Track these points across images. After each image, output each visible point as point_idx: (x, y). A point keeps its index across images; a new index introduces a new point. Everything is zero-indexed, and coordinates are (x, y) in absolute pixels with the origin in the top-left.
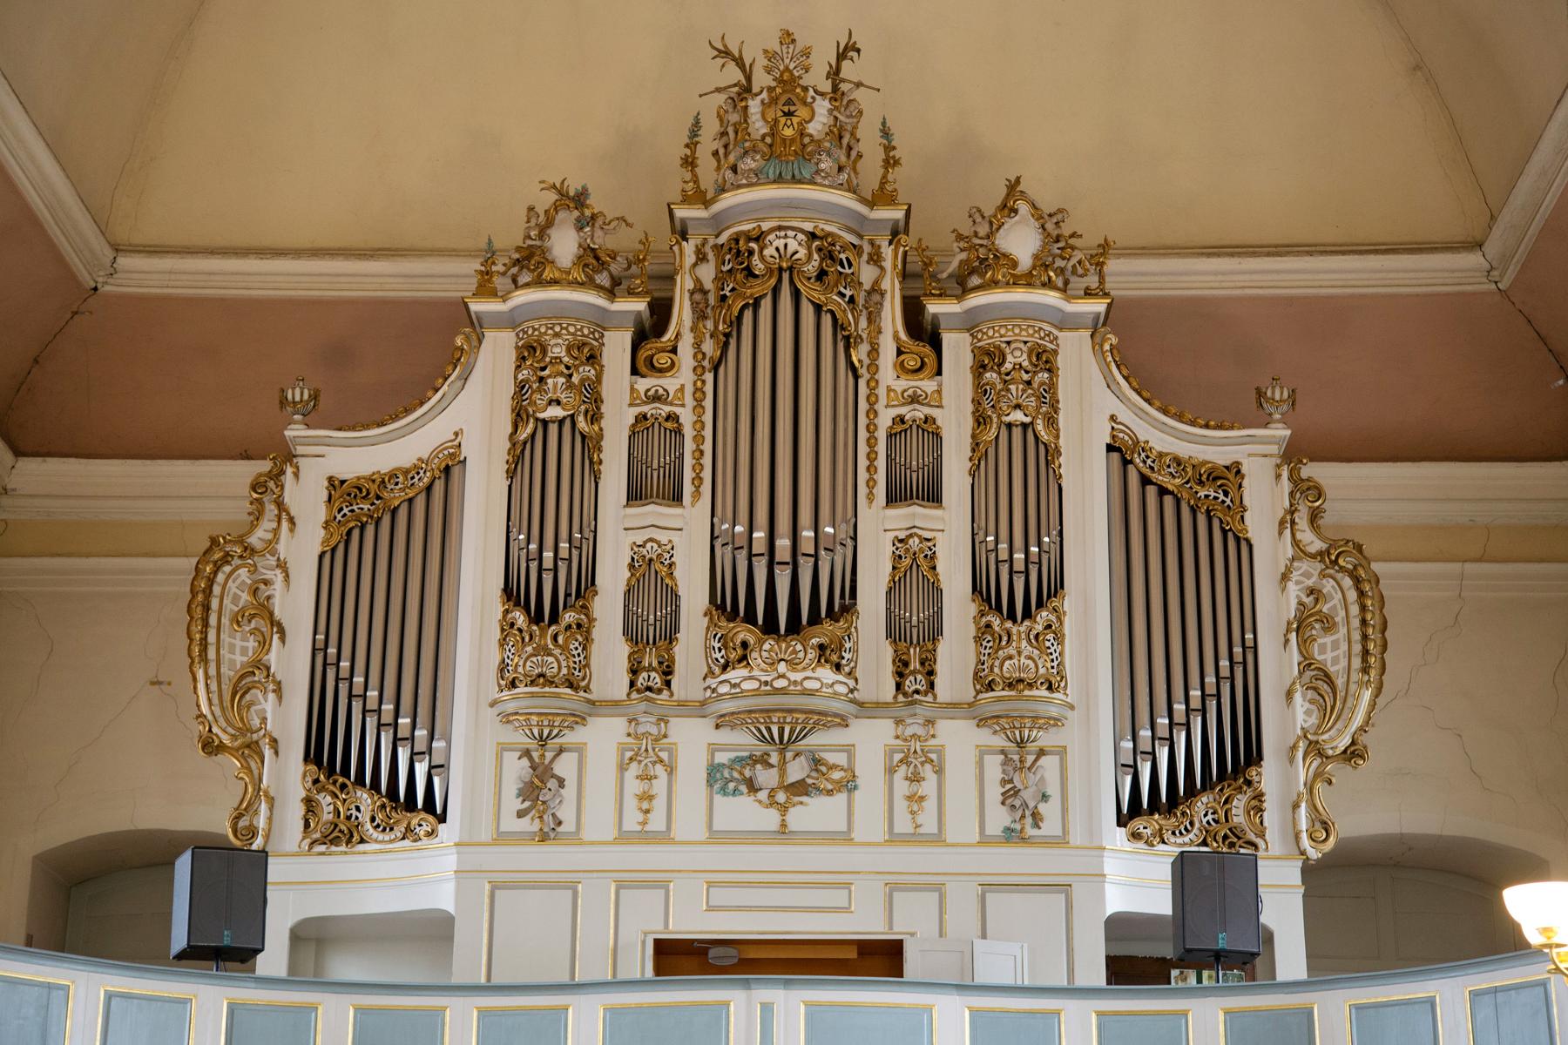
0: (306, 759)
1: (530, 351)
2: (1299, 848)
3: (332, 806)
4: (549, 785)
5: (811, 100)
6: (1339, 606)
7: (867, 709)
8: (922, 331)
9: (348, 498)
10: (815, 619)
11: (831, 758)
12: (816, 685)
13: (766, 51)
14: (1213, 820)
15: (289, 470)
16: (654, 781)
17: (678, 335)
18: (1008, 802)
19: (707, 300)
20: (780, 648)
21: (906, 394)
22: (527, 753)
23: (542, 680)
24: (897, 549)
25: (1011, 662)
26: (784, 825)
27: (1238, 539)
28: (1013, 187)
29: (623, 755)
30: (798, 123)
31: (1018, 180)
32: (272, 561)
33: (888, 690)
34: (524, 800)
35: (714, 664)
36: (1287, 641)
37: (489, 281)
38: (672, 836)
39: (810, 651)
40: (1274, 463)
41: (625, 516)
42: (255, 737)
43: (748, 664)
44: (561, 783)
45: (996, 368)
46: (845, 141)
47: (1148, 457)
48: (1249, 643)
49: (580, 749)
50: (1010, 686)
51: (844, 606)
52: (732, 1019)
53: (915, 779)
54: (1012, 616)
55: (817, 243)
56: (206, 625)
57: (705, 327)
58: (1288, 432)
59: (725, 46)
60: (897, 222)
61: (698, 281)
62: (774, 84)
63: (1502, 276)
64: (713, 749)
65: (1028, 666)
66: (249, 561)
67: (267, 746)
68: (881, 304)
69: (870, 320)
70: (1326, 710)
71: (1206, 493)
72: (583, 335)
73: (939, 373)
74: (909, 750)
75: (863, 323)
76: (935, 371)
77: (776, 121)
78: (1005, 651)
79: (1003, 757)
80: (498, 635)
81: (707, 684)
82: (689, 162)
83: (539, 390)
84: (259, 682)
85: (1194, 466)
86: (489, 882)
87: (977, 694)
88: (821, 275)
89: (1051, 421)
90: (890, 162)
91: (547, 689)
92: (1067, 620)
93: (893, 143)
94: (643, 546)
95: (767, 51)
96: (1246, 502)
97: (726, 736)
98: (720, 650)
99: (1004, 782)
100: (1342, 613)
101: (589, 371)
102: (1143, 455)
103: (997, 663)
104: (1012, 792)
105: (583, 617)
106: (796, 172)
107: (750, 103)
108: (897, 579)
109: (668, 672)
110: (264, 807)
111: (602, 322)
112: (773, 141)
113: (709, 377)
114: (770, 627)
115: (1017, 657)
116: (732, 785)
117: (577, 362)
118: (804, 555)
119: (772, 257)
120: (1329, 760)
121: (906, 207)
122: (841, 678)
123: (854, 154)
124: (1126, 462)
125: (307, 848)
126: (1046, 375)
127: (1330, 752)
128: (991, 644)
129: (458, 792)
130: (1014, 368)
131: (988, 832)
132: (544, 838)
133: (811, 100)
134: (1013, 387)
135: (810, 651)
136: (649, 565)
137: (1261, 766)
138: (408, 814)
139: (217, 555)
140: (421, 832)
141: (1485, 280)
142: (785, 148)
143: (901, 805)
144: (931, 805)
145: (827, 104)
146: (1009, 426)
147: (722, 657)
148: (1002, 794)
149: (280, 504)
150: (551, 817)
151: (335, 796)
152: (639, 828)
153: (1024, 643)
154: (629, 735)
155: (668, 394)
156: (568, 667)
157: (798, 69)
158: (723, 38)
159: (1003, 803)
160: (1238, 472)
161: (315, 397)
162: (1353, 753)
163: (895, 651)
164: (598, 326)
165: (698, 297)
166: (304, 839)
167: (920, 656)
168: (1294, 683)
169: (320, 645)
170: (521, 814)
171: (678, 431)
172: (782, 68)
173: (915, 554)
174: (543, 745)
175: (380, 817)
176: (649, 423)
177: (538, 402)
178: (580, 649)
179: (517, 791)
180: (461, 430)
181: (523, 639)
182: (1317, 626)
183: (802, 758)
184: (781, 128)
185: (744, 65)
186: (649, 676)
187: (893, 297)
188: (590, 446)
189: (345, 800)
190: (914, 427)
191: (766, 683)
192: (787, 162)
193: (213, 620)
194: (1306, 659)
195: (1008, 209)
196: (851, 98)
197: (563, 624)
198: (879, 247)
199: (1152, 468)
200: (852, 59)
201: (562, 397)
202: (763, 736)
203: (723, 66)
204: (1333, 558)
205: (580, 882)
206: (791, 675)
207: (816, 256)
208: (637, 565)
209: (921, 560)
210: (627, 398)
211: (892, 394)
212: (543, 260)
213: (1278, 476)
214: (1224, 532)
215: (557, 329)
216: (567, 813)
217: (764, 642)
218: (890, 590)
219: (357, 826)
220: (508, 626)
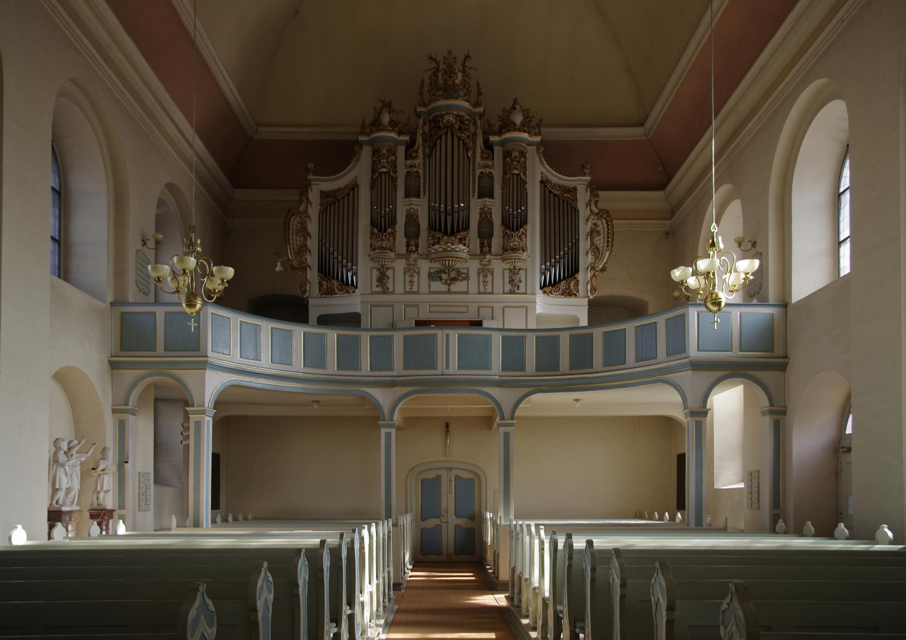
8: (489, 147)
10: (458, 231)
11: (462, 271)
15: (309, 189)
17: (418, 148)
22: (378, 269)
28: (515, 101)
36: (587, 238)
48: (577, 239)
51: (467, 227)
61: (424, 131)
63: (648, 134)
69: (473, 143)
73: (493, 159)
75: (471, 144)
77: (446, 79)
82: (421, 94)
90: (479, 94)
99: (509, 277)
100: (602, 231)
101: (393, 158)
102: (550, 184)
109: (417, 246)
113: (427, 160)
114: (446, 233)
116: (435, 278)
122: (465, 248)
123: (469, 90)
124: (545, 186)
134: (514, 163)
143: (481, 284)
145: (461, 74)
146: (513, 174)
149: (308, 199)
151: (327, 281)
153: (516, 238)
170: (377, 286)
171: (419, 176)
188: (394, 180)
193: (291, 232)
201: (386, 165)
213: (587, 191)
214: (571, 207)
215: (384, 145)
216: (390, 286)
220: (372, 233)
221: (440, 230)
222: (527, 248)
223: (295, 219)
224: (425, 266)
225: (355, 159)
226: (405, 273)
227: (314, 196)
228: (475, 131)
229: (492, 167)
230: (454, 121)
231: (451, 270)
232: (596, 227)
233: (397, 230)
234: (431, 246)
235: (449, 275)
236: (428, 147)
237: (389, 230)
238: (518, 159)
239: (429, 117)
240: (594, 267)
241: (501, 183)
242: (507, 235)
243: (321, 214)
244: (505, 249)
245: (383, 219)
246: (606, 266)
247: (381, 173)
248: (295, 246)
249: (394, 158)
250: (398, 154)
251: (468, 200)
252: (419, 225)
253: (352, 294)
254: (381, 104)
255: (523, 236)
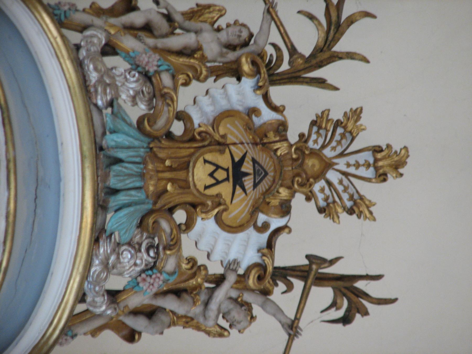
5: (259, 224)
30: (219, 195)
59: (351, 21)
62: (293, 137)
95: (359, 118)
106: (122, 198)
112: (180, 140)
133: (259, 224)
142: (171, 169)
157: (327, 191)
158: (367, 14)
172: (328, 152)
184: (209, 157)
192: (142, 176)
196: (257, 310)
203: (311, 17)
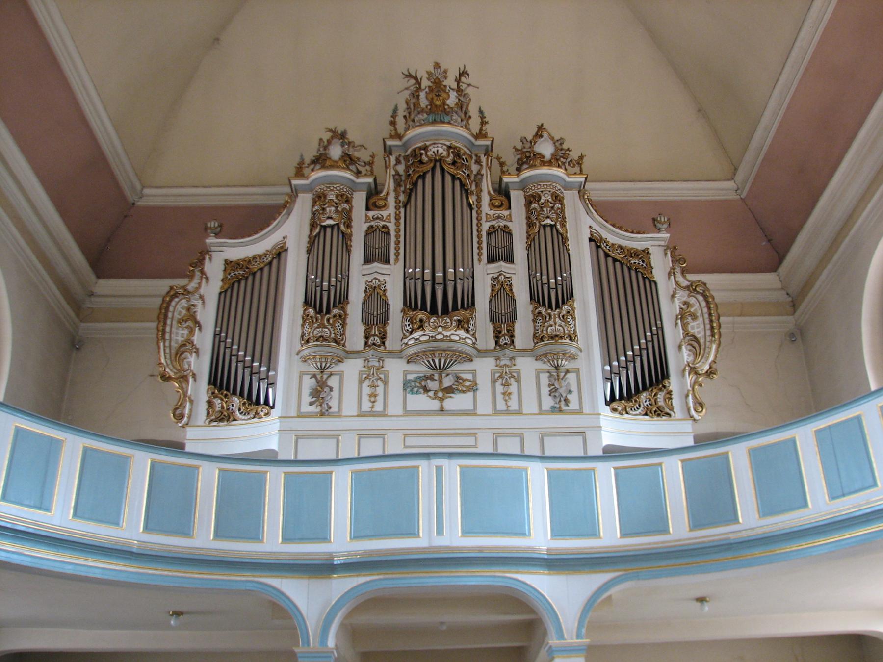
0: (209, 383)
1: (319, 198)
2: (689, 414)
3: (220, 405)
4: (325, 390)
6: (698, 309)
7: (483, 353)
8: (503, 193)
9: (233, 268)
10: (455, 308)
11: (464, 376)
12: (457, 338)
13: (427, 72)
14: (650, 404)
15: (207, 257)
16: (377, 388)
17: (388, 194)
18: (552, 394)
19: (401, 179)
20: (439, 321)
21: (495, 216)
22: (314, 376)
23: (321, 339)
24: (494, 282)
25: (552, 328)
26: (442, 407)
27: (650, 281)
28: (540, 128)
29: (362, 376)
31: (542, 125)
32: (197, 296)
33: (492, 344)
34: (313, 397)
35: (407, 332)
36: (676, 324)
37: (301, 171)
38: (386, 413)
39: (454, 322)
40: (663, 249)
41: (363, 269)
42: (186, 373)
43: (423, 328)
44: (331, 389)
45: (536, 202)
46: (464, 109)
47: (607, 245)
48: (659, 326)
49: (341, 374)
50: (552, 338)
51: (471, 305)
52: (420, 475)
53: (506, 384)
54: (550, 307)
55: (452, 150)
56: (165, 324)
57: (400, 189)
58: (668, 235)
59: (409, 73)
60: (487, 146)
61: (396, 171)
62: (431, 85)
63: (742, 192)
64: (406, 373)
65: (560, 329)
66: (187, 296)
67: (191, 377)
68: (482, 180)
69: (477, 186)
70: (696, 354)
71: (634, 261)
72: (344, 191)
73: (510, 208)
74: (503, 372)
75: (474, 188)
76: (507, 207)
77: (432, 99)
78: (549, 323)
79: (548, 374)
80: (301, 321)
81: (403, 343)
82: (393, 123)
83: (323, 214)
84: (188, 349)
85: (628, 250)
86: (295, 436)
87: (535, 344)
88: (454, 163)
89: (563, 225)
90: (483, 123)
91: (324, 343)
92: (576, 311)
93: (485, 116)
94: (371, 282)
96: (653, 265)
97: (412, 367)
98: (409, 325)
99: (550, 386)
100: (700, 312)
101: (346, 206)
102: (605, 244)
103: (545, 329)
104: (554, 390)
105: (342, 312)
106: (442, 119)
107: (421, 93)
108: (494, 295)
109: (383, 338)
110: (188, 404)
111: (354, 187)
113: (402, 210)
114: (433, 312)
115: (554, 326)
116: (415, 389)
117: (341, 202)
118: (449, 280)
119: (432, 155)
120: (700, 376)
121: (491, 139)
122: (468, 336)
123: (467, 116)
124: (598, 247)
125: (208, 423)
126: (560, 206)
127: (701, 372)
128: (541, 321)
129: (278, 395)
130: (545, 201)
131: (543, 408)
132: (322, 414)
134: (545, 209)
135: (454, 322)
136: (374, 290)
137: (669, 379)
138: (257, 406)
139: (172, 293)
140: (262, 414)
141: (735, 194)
143: (500, 398)
144: (515, 397)
145: (455, 93)
146: (545, 226)
147: (410, 328)
148: (549, 391)
149: (202, 272)
150: (326, 405)
151: (222, 399)
152: (370, 410)
153: (557, 319)
154: (365, 367)
155: (383, 217)
156: (334, 334)
159: (550, 395)
160: (648, 253)
161: (221, 226)
162: (711, 372)
163: (494, 327)
164: (351, 189)
165: (397, 177)
166: (207, 419)
167: (506, 328)
168: (682, 341)
169: (217, 333)
170: (311, 404)
171: (388, 233)
173: (502, 282)
174: (322, 372)
175: (243, 408)
176: (374, 229)
177: (322, 218)
178: (341, 327)
179: (309, 393)
180: (286, 236)
181: (313, 321)
182: (689, 318)
183: (450, 376)
185: (417, 79)
186: (374, 339)
187: (487, 176)
188: (346, 238)
189: (227, 401)
190: (499, 230)
191: (432, 337)
193: (169, 322)
194: (685, 331)
195: (538, 135)
196: (466, 92)
197: (332, 314)
198: (480, 157)
199: (609, 250)
200: (465, 77)
201: (334, 216)
202: (431, 366)
204: (694, 287)
205: (340, 435)
206: (444, 333)
207: (451, 155)
208: (368, 290)
209: (505, 286)
210: (364, 219)
211: (488, 216)
212: (325, 158)
213: (666, 254)
214: (644, 278)
215: (332, 188)
216: (334, 403)
217: (431, 318)
218: (491, 301)
219: (232, 413)
220: (305, 317)
221: (424, 308)
222: (576, 336)
223: (179, 301)
224: (396, 369)
225: (284, 213)
226: (361, 382)
227: (214, 268)
228: (479, 173)
229: (509, 218)
230: (445, 153)
231: (444, 375)
232: (688, 307)
233: (349, 312)
234: (408, 334)
235: (441, 382)
236: (404, 192)
237: (335, 311)
238: (551, 205)
239: (405, 153)
240: (694, 368)
241: (526, 240)
242: (542, 316)
243: (223, 295)
244: (538, 338)
245: (325, 294)
246: (714, 366)
247: (325, 227)
248: (173, 344)
249: (348, 207)
250: (355, 202)
251: (471, 266)
252: (387, 304)
253: (265, 419)
254: (330, 134)
255: (569, 317)
